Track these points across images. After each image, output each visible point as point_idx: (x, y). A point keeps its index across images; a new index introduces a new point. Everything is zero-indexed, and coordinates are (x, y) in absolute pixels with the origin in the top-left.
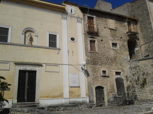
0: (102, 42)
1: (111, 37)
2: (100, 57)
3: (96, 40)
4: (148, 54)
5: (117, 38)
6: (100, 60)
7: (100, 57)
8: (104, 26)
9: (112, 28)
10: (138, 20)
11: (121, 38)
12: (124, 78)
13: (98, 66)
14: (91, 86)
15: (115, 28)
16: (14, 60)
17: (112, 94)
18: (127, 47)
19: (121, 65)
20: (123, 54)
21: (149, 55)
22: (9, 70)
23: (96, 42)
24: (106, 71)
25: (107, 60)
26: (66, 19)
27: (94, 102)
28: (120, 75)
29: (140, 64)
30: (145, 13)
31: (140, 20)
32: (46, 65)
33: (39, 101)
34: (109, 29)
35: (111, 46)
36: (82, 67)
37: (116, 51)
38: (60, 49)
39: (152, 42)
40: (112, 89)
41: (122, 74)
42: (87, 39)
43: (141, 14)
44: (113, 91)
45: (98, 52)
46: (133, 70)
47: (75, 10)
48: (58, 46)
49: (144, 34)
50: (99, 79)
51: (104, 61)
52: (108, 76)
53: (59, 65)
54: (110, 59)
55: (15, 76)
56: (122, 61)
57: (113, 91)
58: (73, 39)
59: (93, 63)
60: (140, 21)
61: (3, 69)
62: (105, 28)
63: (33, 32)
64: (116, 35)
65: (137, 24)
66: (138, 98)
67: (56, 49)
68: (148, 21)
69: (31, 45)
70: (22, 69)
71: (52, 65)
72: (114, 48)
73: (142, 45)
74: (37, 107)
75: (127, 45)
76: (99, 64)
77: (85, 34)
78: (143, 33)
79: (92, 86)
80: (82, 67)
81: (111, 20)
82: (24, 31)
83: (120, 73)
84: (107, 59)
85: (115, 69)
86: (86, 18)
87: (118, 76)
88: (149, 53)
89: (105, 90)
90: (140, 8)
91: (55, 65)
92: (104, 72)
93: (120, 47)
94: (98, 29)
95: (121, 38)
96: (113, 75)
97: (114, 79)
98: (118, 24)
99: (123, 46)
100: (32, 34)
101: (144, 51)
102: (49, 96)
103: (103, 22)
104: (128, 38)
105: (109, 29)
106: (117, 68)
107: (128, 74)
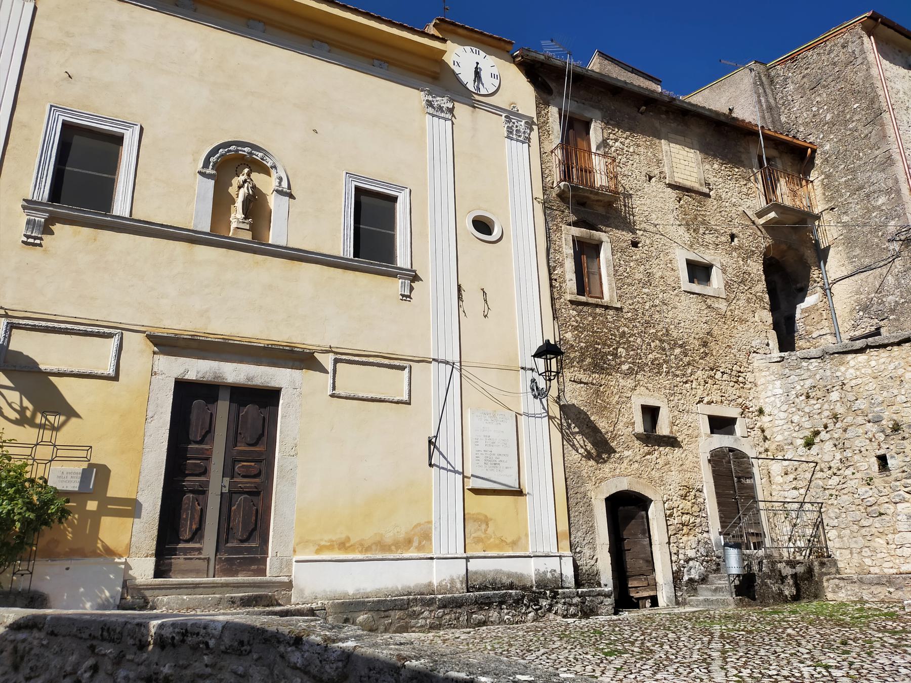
0: (638, 254)
1: (682, 230)
2: (626, 329)
3: (603, 236)
4: (873, 329)
5: (709, 238)
6: (629, 347)
7: (626, 329)
8: (645, 170)
9: (688, 184)
10: (814, 151)
11: (733, 236)
12: (746, 447)
13: (617, 381)
14: (582, 489)
15: (701, 185)
16: (147, 321)
17: (692, 540)
18: (761, 286)
19: (738, 379)
20: (742, 321)
21: (878, 329)
22: (116, 378)
23: (605, 253)
24: (659, 408)
25: (664, 349)
26: (449, 116)
27: (599, 585)
28: (731, 432)
29: (851, 371)
30: (854, 112)
31: (827, 147)
32: (339, 357)
33: (290, 570)
34: (670, 186)
35: (684, 273)
36: (533, 381)
37: (709, 307)
38: (415, 278)
39: (898, 262)
40: (696, 508)
41: (739, 428)
42: (559, 229)
43: (829, 117)
44: (698, 520)
45: (619, 305)
46: (807, 410)
47: (495, 71)
48: (402, 260)
49: (845, 225)
50: (626, 453)
51: (650, 356)
52: (668, 437)
53: (411, 363)
54: (680, 342)
55: (150, 414)
56: (742, 357)
57: (698, 520)
58: (483, 226)
59: (589, 360)
60: (825, 153)
61: (76, 370)
62: (650, 178)
63: (266, 171)
64: (703, 223)
65: (807, 173)
66: (841, 565)
67: (394, 275)
68: (877, 152)
69: (249, 238)
70: (191, 376)
71: (371, 360)
72: (696, 288)
73: (836, 281)
74: (278, 608)
75: (763, 277)
76: (625, 367)
77: (547, 206)
78: (845, 219)
79: (589, 486)
80: (533, 381)
81: (675, 148)
82: (213, 159)
83: (732, 421)
84: (660, 341)
85: (709, 403)
86: (551, 120)
87: (721, 441)
88: (882, 323)
89: (655, 513)
90: (824, 87)
91: (386, 362)
92: (651, 413)
93: (728, 286)
94: (870, 38)
95: (733, 236)
96: (695, 433)
97: (704, 457)
98: (716, 166)
99: (744, 279)
100: (258, 178)
101: (848, 310)
102: (348, 539)
103: (638, 146)
104: (764, 242)
105: (670, 186)
106: (716, 397)
107: (775, 430)
